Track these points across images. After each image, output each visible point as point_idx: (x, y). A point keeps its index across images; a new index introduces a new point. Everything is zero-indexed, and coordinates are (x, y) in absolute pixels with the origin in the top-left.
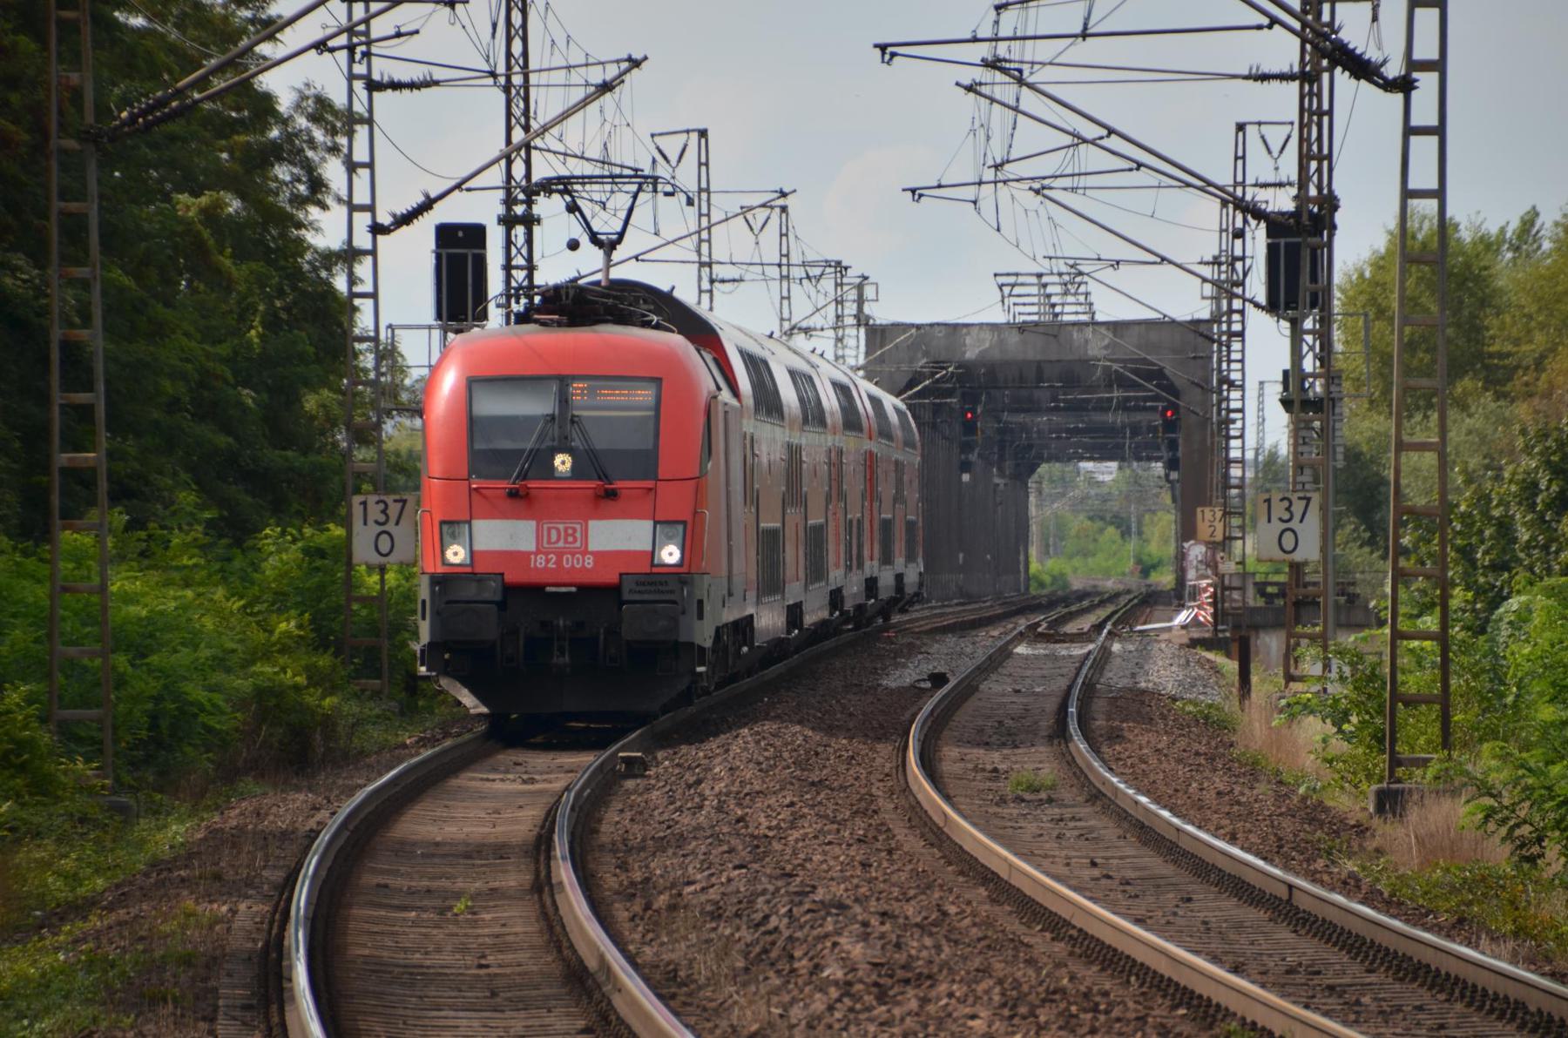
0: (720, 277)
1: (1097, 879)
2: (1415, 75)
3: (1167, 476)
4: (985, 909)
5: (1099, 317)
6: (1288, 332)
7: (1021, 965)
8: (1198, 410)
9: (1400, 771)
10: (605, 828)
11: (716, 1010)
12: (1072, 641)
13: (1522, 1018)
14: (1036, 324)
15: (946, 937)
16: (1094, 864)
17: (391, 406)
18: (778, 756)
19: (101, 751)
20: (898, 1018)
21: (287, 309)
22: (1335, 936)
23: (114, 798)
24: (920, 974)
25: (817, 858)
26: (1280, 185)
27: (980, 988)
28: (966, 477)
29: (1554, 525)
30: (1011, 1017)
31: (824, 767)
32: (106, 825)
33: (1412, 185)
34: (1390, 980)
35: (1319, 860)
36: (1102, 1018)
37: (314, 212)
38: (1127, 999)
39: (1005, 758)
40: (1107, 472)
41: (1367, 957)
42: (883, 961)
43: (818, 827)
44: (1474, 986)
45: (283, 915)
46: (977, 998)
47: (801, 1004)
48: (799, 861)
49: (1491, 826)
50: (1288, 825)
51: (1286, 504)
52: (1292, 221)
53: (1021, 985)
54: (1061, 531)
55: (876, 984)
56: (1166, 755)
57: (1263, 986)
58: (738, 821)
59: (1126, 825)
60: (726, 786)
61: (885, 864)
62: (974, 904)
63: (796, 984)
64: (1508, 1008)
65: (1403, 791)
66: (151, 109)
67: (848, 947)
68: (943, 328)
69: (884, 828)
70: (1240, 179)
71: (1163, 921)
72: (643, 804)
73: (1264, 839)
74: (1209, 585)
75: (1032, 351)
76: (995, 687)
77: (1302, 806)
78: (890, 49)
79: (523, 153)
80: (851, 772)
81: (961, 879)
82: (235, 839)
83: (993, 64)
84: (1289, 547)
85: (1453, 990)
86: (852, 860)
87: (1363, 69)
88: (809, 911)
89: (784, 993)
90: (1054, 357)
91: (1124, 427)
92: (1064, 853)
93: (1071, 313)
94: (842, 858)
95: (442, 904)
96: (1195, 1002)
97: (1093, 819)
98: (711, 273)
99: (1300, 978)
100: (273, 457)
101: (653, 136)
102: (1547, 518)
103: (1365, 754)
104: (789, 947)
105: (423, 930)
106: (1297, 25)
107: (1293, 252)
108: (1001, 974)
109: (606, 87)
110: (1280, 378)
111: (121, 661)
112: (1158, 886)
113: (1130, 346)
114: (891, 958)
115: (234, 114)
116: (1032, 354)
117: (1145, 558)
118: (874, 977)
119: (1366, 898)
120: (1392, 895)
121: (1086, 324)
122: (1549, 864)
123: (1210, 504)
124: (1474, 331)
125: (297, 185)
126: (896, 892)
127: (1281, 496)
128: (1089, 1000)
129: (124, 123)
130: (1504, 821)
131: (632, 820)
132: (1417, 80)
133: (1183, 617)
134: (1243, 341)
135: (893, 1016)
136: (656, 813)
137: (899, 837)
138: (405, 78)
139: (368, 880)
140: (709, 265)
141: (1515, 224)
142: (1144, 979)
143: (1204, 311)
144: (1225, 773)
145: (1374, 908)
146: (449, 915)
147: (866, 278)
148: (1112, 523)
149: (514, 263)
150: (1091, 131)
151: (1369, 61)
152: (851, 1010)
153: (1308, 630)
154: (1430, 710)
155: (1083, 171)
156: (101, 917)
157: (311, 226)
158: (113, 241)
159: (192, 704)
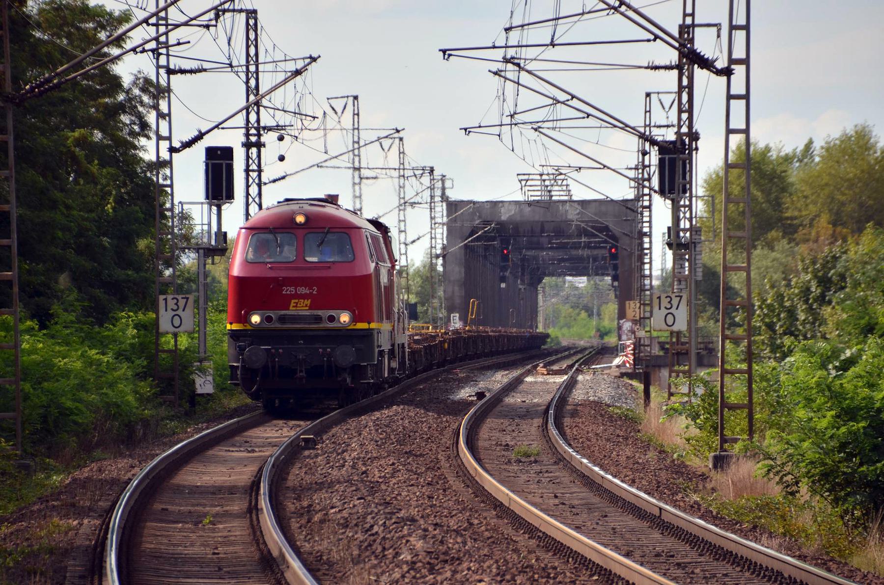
0: (365, 176)
1: (557, 505)
2: (733, 67)
4: (493, 522)
5: (575, 198)
6: (670, 206)
9: (726, 446)
10: (291, 477)
11: (341, 578)
12: (556, 374)
13: (780, 581)
14: (538, 201)
15: (470, 537)
16: (556, 497)
17: (185, 245)
20: (439, 581)
21: (128, 193)
22: (683, 535)
23: (22, 461)
24: (453, 557)
25: (404, 494)
26: (668, 126)
27: (485, 565)
28: (503, 285)
29: (818, 310)
31: (413, 444)
32: (17, 476)
33: (732, 127)
34: (711, 560)
37: (143, 141)
38: (566, 571)
39: (514, 438)
40: (581, 282)
41: (699, 547)
43: (407, 476)
44: (756, 563)
45: (105, 528)
46: (484, 571)
47: (387, 574)
48: (394, 495)
49: (771, 475)
50: (663, 475)
51: (669, 299)
52: (671, 146)
53: (508, 563)
54: (557, 314)
55: (429, 563)
56: (601, 437)
57: (642, 565)
58: (363, 473)
61: (441, 497)
63: (385, 563)
65: (728, 456)
66: (42, 84)
67: (414, 543)
70: (648, 123)
71: (591, 528)
73: (650, 483)
74: (631, 344)
75: (538, 216)
76: (514, 399)
77: (672, 464)
78: (448, 52)
79: (255, 108)
80: (428, 446)
81: (482, 505)
82: (84, 484)
83: (506, 61)
84: (670, 323)
85: (744, 565)
86: (423, 495)
87: (706, 64)
88: (395, 523)
89: (378, 568)
90: (549, 219)
91: (588, 257)
92: (540, 491)
93: (558, 195)
94: (418, 494)
95: (197, 520)
96: (603, 572)
98: (360, 175)
99: (662, 559)
100: (120, 274)
101: (328, 99)
102: (814, 307)
105: (185, 534)
106: (677, 45)
107: (673, 162)
108: (497, 557)
109: (298, 73)
110: (666, 231)
111: (27, 387)
112: (590, 509)
113: (590, 214)
117: (602, 329)
118: (428, 559)
119: (702, 515)
120: (718, 513)
121: (565, 202)
124: (777, 204)
126: (446, 512)
127: (666, 295)
128: (545, 572)
129: (27, 92)
130: (778, 473)
131: (306, 473)
133: (617, 361)
134: (650, 211)
135: (437, 580)
136: (319, 469)
138: (188, 67)
139: (158, 506)
140: (359, 169)
141: (801, 147)
142: (576, 560)
143: (630, 195)
147: (444, 176)
148: (582, 309)
149: (251, 168)
150: (563, 97)
151: (707, 59)
152: (414, 577)
153: (682, 368)
154: (742, 412)
157: (143, 148)
158: (25, 157)
159: (67, 409)
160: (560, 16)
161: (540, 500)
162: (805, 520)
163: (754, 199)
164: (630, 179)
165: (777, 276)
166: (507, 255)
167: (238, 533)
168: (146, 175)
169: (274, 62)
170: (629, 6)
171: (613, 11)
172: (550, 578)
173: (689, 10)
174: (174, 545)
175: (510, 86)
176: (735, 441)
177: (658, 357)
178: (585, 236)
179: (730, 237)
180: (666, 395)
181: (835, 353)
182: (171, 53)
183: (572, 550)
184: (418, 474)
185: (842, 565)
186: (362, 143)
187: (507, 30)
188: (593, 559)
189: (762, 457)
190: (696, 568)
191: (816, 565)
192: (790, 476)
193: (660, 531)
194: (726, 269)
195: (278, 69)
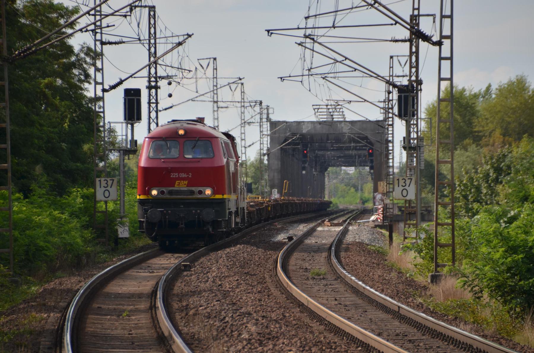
0: (221, 106)
1: (337, 305)
2: (443, 40)
3: (370, 171)
4: (298, 315)
5: (347, 120)
6: (405, 124)
7: (308, 333)
8: (379, 150)
9: (439, 269)
10: (176, 288)
12: (336, 226)
14: (325, 122)
15: (284, 324)
16: (336, 300)
18: (234, 264)
19: (9, 263)
20: (265, 351)
21: (77, 117)
22: (413, 323)
23: (13, 278)
24: (274, 336)
25: (244, 298)
26: (403, 76)
27: (293, 341)
28: (304, 172)
29: (494, 187)
30: (303, 351)
31: (250, 268)
32: (10, 287)
33: (442, 76)
34: (430, 338)
35: (410, 298)
36: (333, 351)
37: (86, 85)
38: (342, 345)
40: (351, 170)
41: (423, 330)
42: (261, 332)
43: (246, 287)
44: (456, 340)
45: (63, 319)
46: (292, 344)
47: (234, 346)
48: (238, 299)
49: (466, 287)
50: (401, 287)
51: (404, 181)
52: (406, 88)
55: (259, 340)
56: (363, 264)
57: (388, 341)
58: (219, 286)
59: (347, 287)
60: (216, 274)
61: (267, 300)
62: (295, 313)
63: (233, 340)
64: (467, 347)
65: (439, 275)
66: (25, 51)
68: (295, 123)
69: (268, 288)
70: (391, 74)
72: (189, 280)
73: (393, 291)
74: (381, 207)
75: (325, 130)
76: (310, 241)
78: (270, 32)
79: (154, 65)
80: (258, 269)
82: (51, 292)
83: (306, 37)
84: (405, 195)
85: (450, 341)
86: (256, 299)
87: (427, 39)
88: (238, 315)
90: (332, 132)
91: (355, 156)
92: (326, 296)
93: (337, 118)
94: (252, 298)
95: (119, 313)
96: (364, 345)
97: (338, 285)
99: (400, 338)
100: (73, 165)
101: (198, 60)
102: (492, 185)
103: (427, 263)
104: (231, 327)
105: (112, 322)
106: (409, 27)
107: (406, 98)
109: (180, 44)
110: (402, 139)
111: (16, 233)
112: (356, 307)
113: (356, 129)
114: (264, 331)
115: (59, 53)
116: (325, 131)
117: (364, 199)
118: (258, 337)
120: (434, 310)
121: (341, 122)
122: (485, 299)
123: (383, 181)
124: (470, 123)
125: (80, 76)
126: (269, 309)
127: (402, 178)
128: (329, 345)
129: (16, 55)
131: (185, 285)
132: (443, 42)
133: (373, 218)
134: (393, 127)
135: (264, 350)
136: (193, 283)
137: (272, 291)
138: (113, 41)
139: (95, 306)
141: (484, 89)
142: (348, 338)
143: (381, 117)
144: (382, 269)
145: (426, 314)
146: (121, 317)
147: (268, 106)
149: (151, 101)
150: (340, 58)
151: (427, 36)
152: (250, 348)
153: (412, 222)
155: (337, 71)
156: (4, 318)
157: (86, 89)
159: (40, 247)
160: (339, 9)
161: (326, 302)
162: (486, 314)
163: (456, 120)
164: (381, 108)
165: (469, 167)
166: (306, 154)
167: (143, 322)
168: (88, 106)
169: (166, 37)
170: (380, 4)
171: (370, 7)
172: (332, 349)
173: (416, 6)
174: (105, 329)
175: (308, 52)
176: (444, 266)
177: (398, 215)
178: (354, 142)
179: (441, 143)
180: (402, 238)
181: (505, 213)
182: (103, 32)
183: (345, 332)
184: (253, 286)
185: (508, 341)
186: (219, 86)
187: (307, 18)
188: (358, 337)
189: (460, 276)
190: (421, 343)
191: (493, 341)
192: (477, 288)
193: (399, 321)
194: (438, 162)
195: (168, 42)
